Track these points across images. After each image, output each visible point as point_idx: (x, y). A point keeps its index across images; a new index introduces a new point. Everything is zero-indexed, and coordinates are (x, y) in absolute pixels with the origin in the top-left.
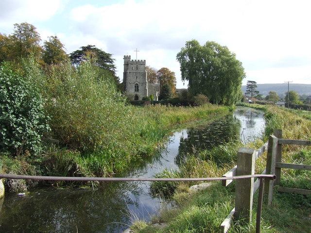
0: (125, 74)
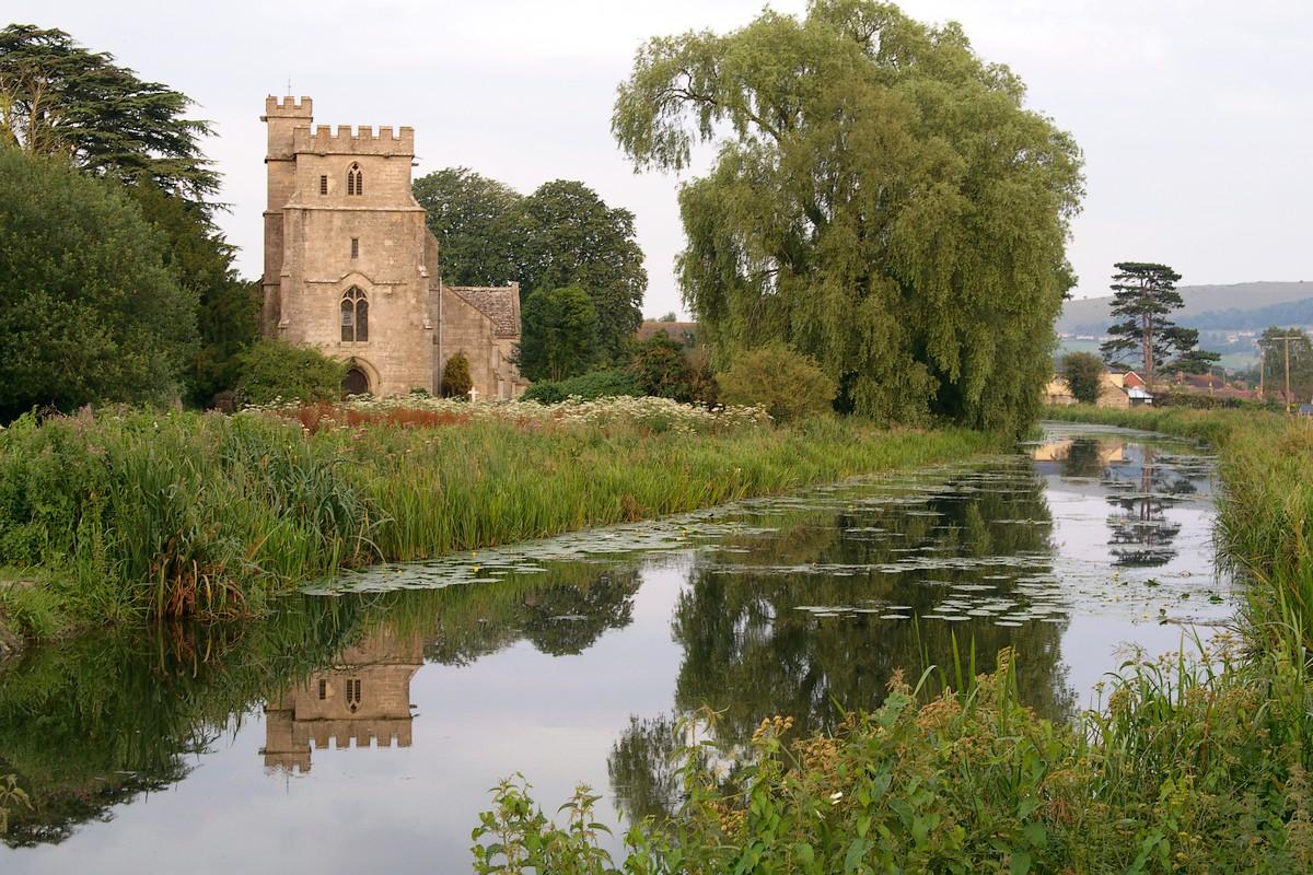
0: (274, 222)
